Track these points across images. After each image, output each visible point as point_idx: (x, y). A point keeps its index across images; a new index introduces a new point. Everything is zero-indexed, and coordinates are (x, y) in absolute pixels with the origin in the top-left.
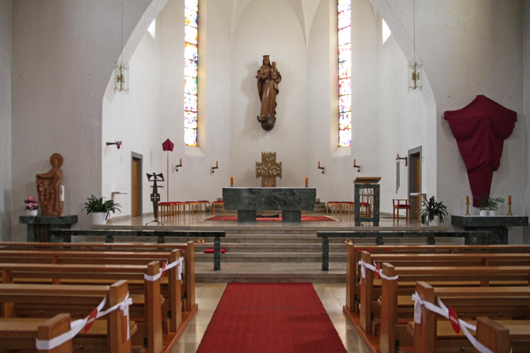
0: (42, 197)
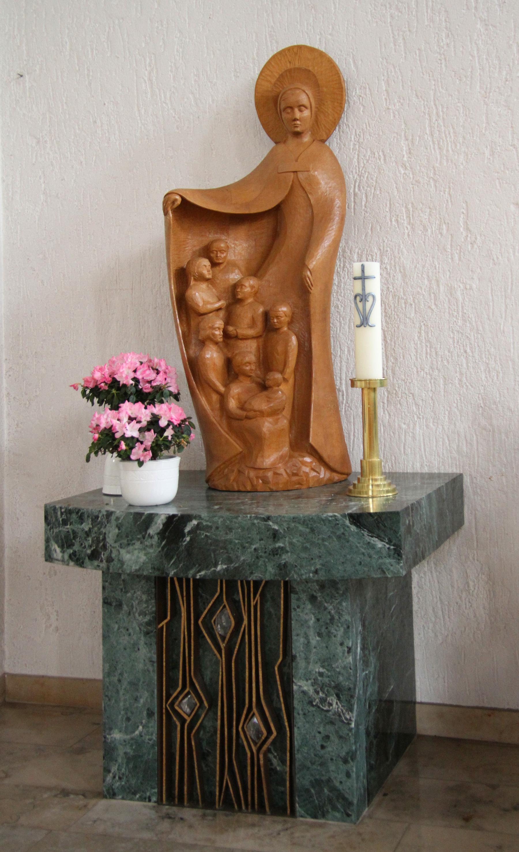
0: (212, 356)
